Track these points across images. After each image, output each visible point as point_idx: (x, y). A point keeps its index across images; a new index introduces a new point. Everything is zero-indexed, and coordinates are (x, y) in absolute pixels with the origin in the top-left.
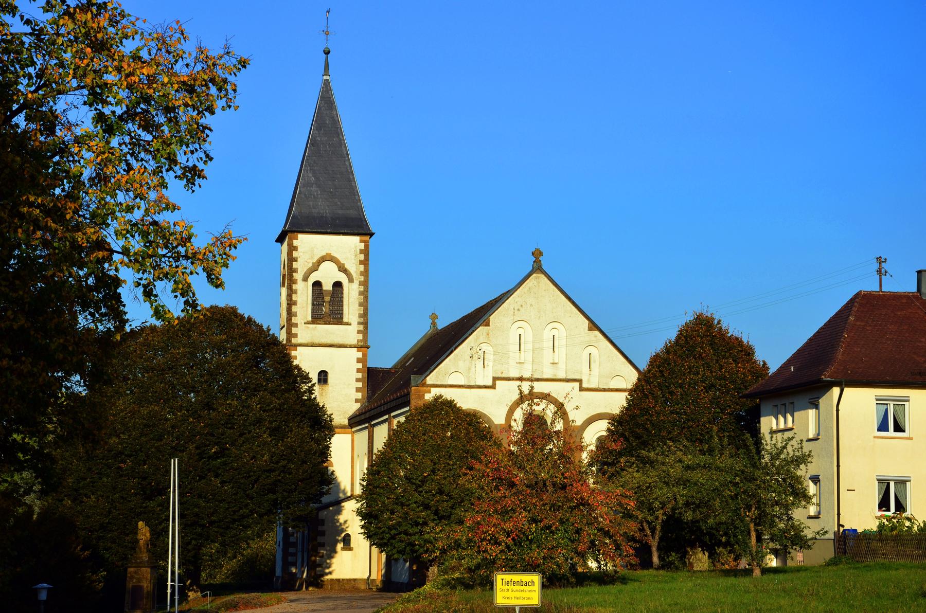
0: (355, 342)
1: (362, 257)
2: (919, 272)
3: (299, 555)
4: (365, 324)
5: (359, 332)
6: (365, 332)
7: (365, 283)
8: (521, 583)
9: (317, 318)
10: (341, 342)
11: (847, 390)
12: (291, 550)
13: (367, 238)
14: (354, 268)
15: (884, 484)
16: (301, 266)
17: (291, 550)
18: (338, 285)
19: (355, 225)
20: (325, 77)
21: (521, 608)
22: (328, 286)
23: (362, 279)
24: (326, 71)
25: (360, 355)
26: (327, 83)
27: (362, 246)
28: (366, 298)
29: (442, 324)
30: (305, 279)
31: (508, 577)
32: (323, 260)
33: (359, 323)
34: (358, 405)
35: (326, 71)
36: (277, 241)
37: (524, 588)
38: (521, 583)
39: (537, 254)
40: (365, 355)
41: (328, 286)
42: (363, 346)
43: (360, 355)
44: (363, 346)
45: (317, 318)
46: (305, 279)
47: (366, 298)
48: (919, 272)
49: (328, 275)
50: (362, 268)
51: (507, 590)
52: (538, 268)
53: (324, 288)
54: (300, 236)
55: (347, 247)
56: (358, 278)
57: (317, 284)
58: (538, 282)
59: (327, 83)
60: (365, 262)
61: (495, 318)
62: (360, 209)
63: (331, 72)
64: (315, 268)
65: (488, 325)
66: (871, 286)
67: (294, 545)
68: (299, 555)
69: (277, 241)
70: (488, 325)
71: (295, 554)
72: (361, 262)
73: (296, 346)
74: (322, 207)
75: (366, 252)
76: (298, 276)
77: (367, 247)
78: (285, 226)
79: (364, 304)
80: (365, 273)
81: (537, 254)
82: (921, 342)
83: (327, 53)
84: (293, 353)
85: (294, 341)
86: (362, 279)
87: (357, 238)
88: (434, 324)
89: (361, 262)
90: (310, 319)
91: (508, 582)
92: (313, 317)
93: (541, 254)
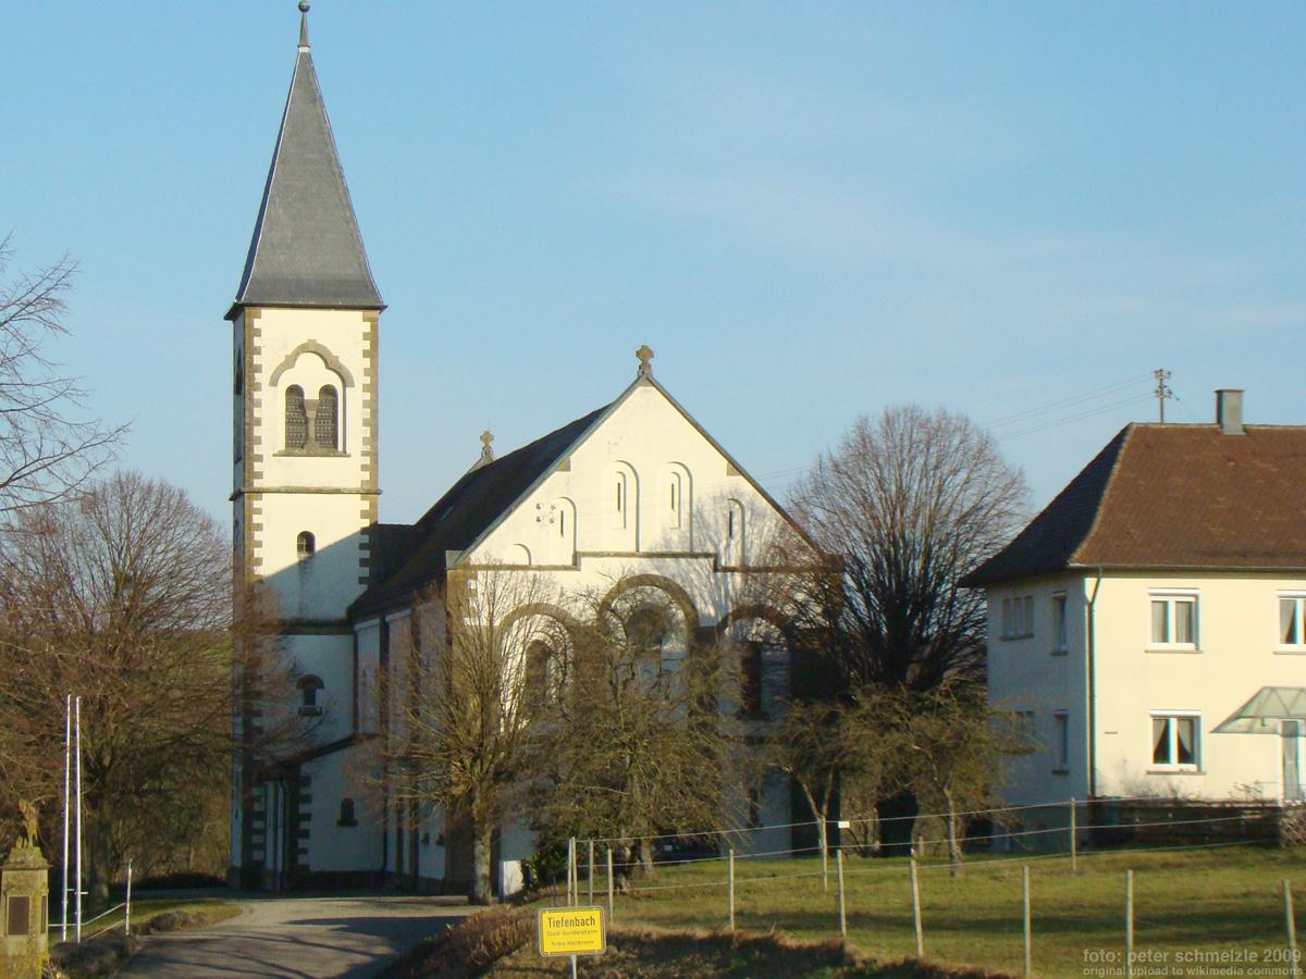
0: (357, 485)
1: (367, 345)
2: (1220, 393)
3: (270, 832)
4: (374, 455)
5: (364, 468)
6: (373, 468)
7: (372, 388)
8: (576, 922)
9: (297, 442)
10: (335, 485)
11: (1105, 581)
12: (257, 824)
13: (375, 314)
14: (357, 365)
15: (1163, 724)
16: (267, 357)
17: (257, 824)
18: (328, 391)
19: (360, 296)
20: (302, 50)
21: (578, 957)
22: (312, 394)
23: (368, 380)
24: (303, 41)
25: (366, 505)
26: (306, 60)
27: (367, 327)
28: (374, 413)
29: (500, 451)
30: (274, 382)
31: (558, 915)
32: (303, 349)
33: (364, 454)
34: (363, 588)
35: (303, 41)
36: (227, 318)
37: (581, 928)
38: (576, 922)
39: (644, 354)
40: (373, 506)
41: (312, 394)
42: (370, 491)
43: (366, 505)
44: (370, 491)
45: (297, 442)
46: (274, 382)
47: (374, 413)
48: (1220, 393)
49: (312, 377)
50: (367, 362)
51: (558, 934)
52: (645, 377)
53: (307, 397)
54: (265, 312)
55: (343, 330)
56: (360, 379)
57: (294, 392)
58: (645, 396)
59: (306, 60)
60: (372, 354)
61: (583, 455)
62: (363, 265)
63: (311, 38)
64: (290, 362)
65: (568, 468)
66: (1146, 413)
67: (262, 816)
68: (270, 832)
69: (227, 318)
70: (568, 468)
71: (262, 832)
72: (366, 354)
73: (260, 492)
74: (305, 264)
75: (373, 337)
76: (262, 378)
77: (374, 328)
78: (239, 297)
79: (373, 423)
80: (373, 371)
81: (644, 354)
82: (1219, 503)
83: (303, 9)
84: (256, 504)
85: (257, 484)
86: (368, 380)
87: (359, 314)
88: (487, 451)
89: (366, 354)
90: (282, 446)
91: (558, 922)
92: (287, 445)
93: (651, 354)
